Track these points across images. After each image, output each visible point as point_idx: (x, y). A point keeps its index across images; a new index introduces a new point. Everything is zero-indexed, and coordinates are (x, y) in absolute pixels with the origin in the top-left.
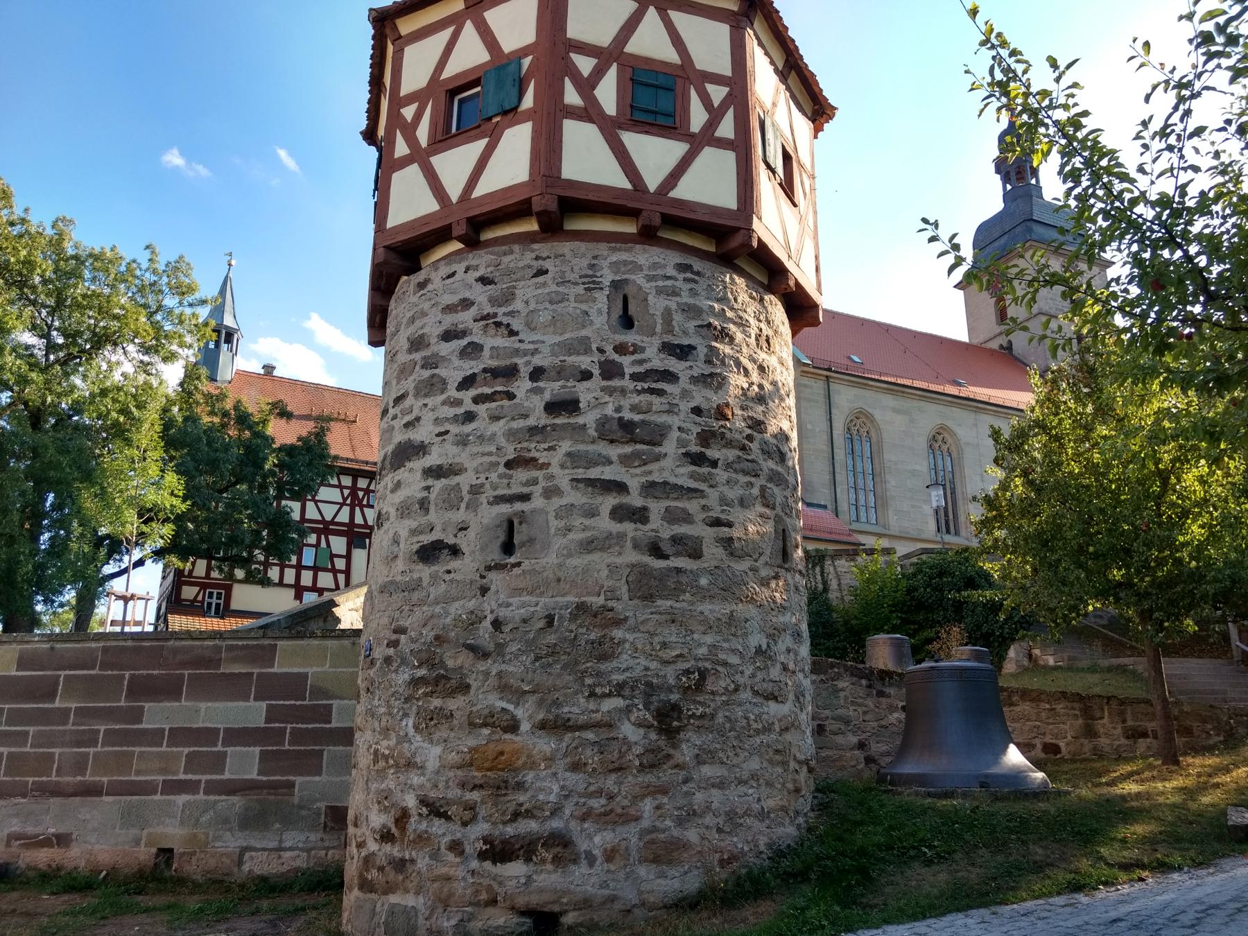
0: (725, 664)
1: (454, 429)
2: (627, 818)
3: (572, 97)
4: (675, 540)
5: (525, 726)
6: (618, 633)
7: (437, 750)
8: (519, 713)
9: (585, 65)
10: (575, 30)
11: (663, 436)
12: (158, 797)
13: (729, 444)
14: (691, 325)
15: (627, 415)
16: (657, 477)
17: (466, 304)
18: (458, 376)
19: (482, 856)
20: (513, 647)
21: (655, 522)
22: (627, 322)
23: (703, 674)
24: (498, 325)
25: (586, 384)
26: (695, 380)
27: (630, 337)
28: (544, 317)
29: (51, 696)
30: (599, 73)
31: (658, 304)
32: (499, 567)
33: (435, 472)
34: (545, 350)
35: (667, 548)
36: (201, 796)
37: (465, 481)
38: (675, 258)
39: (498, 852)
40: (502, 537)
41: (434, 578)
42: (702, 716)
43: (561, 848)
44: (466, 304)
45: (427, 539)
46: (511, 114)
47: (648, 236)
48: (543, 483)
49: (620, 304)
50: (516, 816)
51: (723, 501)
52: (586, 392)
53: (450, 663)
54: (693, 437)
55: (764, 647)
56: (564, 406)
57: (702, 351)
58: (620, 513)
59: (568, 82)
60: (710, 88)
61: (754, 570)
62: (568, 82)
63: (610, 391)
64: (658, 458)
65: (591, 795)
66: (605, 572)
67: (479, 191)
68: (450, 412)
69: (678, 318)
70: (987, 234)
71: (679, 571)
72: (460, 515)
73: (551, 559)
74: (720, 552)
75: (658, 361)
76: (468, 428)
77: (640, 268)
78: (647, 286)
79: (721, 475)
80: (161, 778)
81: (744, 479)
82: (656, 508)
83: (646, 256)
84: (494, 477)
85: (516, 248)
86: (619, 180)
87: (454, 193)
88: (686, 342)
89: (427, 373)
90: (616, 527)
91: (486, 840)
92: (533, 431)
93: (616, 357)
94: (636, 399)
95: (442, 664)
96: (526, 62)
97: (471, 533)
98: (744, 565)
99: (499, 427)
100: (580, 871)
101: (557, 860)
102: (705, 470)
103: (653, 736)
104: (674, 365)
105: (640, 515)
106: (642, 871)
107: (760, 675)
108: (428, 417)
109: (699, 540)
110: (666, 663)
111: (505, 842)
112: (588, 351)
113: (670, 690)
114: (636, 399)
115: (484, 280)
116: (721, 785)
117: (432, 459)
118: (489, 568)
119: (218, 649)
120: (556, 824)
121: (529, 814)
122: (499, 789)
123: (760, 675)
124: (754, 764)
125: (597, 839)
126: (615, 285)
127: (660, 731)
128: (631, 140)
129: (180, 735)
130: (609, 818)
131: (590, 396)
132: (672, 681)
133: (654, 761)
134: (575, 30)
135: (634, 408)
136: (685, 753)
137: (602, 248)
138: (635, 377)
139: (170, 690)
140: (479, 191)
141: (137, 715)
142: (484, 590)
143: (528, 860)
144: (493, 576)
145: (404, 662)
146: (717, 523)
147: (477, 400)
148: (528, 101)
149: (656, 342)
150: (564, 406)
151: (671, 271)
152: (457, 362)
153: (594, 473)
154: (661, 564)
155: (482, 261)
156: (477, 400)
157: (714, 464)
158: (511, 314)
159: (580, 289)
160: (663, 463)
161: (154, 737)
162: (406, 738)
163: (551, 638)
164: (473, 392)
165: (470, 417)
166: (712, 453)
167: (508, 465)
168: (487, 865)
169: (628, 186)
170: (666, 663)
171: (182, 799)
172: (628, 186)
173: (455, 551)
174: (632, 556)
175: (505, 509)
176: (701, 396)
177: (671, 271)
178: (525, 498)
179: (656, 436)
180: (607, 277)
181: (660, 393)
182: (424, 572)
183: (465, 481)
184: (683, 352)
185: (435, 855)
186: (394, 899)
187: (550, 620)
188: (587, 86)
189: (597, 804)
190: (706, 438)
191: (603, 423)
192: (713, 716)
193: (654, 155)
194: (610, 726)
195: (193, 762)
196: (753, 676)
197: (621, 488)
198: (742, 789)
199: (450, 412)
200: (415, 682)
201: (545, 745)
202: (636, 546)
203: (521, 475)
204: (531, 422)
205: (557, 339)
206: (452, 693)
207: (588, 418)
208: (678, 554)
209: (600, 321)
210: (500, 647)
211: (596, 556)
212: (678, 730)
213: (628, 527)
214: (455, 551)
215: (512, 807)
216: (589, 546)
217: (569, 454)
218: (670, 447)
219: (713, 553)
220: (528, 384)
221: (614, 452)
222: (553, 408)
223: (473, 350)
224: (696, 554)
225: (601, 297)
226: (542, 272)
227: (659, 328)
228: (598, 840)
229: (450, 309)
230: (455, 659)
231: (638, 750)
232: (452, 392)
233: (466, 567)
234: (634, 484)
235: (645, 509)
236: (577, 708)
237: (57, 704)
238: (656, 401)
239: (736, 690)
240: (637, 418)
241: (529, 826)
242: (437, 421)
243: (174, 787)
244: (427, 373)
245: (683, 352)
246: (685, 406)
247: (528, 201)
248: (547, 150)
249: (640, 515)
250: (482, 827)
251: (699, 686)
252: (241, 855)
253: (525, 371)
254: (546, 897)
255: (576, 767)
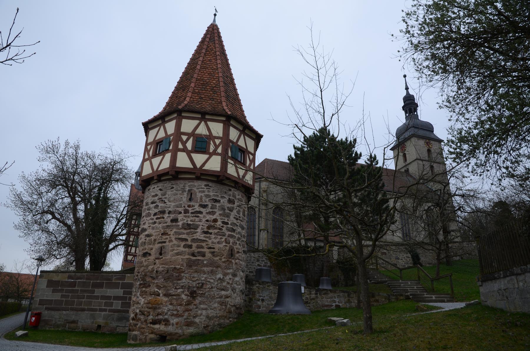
0: (209, 282)
1: (152, 226)
2: (181, 316)
3: (180, 146)
4: (198, 252)
5: (161, 295)
6: (182, 274)
7: (143, 300)
8: (160, 292)
9: (184, 138)
10: (183, 130)
11: (198, 227)
12: (98, 312)
13: (216, 228)
14: (207, 200)
15: (189, 222)
16: (195, 237)
17: (156, 195)
18: (154, 212)
19: (151, 323)
20: (160, 277)
21: (194, 248)
22: (190, 200)
23: (203, 284)
24: (162, 200)
25: (180, 215)
26: (207, 213)
27: (192, 203)
28: (172, 199)
29: (75, 286)
30: (188, 140)
31: (199, 195)
32: (158, 259)
33: (148, 236)
34: (172, 207)
35: (196, 254)
36: (107, 313)
37: (153, 238)
38: (205, 183)
39: (154, 322)
40: (159, 251)
41: (145, 260)
42: (202, 294)
43: (167, 322)
44: (156, 195)
45: (145, 251)
46: (167, 150)
47: (198, 178)
48: (169, 239)
49: (190, 195)
50: (158, 315)
51: (213, 243)
52: (180, 217)
53: (147, 280)
54: (205, 227)
55: (222, 278)
56: (175, 220)
57: (210, 206)
58: (185, 246)
59: (180, 143)
60: (216, 140)
61: (220, 259)
62: (180, 143)
63: (185, 216)
64: (196, 233)
65: (174, 310)
66: (180, 261)
67: (159, 169)
68: (151, 221)
69: (204, 198)
70: (400, 133)
71: (199, 260)
72: (151, 246)
73: (169, 257)
74: (210, 255)
75: (197, 208)
76: (154, 226)
77: (195, 186)
78: (197, 190)
79: (213, 236)
80: (98, 308)
81: (219, 237)
82: (194, 245)
83: (197, 183)
84: (159, 237)
85: (168, 182)
86: (191, 166)
87: (155, 169)
88: (206, 204)
89: (148, 211)
90: (184, 250)
91: (152, 319)
92: (168, 226)
93: (188, 208)
94: (192, 218)
95: (145, 280)
96: (172, 138)
97: (154, 250)
98: (218, 258)
99: (160, 225)
100: (170, 327)
101: (165, 325)
102: (208, 235)
103: (189, 298)
104: (202, 210)
105: (190, 247)
106: (184, 327)
107: (219, 285)
108: (147, 223)
109: (205, 252)
110: (194, 281)
111: (156, 320)
112: (181, 207)
113: (194, 287)
114: (192, 218)
115: (161, 190)
116: (206, 309)
117: (146, 233)
118: (156, 259)
119: (112, 275)
120: (166, 317)
121: (160, 314)
122: (155, 309)
123: (219, 285)
124: (216, 305)
125: (175, 320)
126: (189, 190)
127: (191, 297)
128: (193, 155)
129: (103, 297)
130: (177, 316)
131: (181, 218)
132: (194, 285)
133: (189, 303)
134: (183, 130)
135: (191, 221)
136: (197, 301)
137: (187, 182)
138: (192, 213)
139: (100, 286)
140: (159, 169)
141: (93, 292)
142: (155, 264)
143: (160, 324)
144: (157, 261)
145: (139, 280)
146: (210, 248)
147: (157, 219)
148: (171, 148)
149: (198, 204)
150: (175, 220)
151: (203, 187)
152: (153, 209)
153: (180, 236)
154: (195, 258)
155: (160, 185)
156: (157, 219)
157: (211, 234)
158: (165, 198)
159: (181, 192)
160: (197, 234)
161: (97, 297)
162: (138, 297)
163: (168, 275)
164: (156, 217)
165: (155, 223)
166: (210, 231)
167: (162, 234)
168: (152, 325)
169: (192, 167)
170: (194, 281)
171: (103, 313)
172: (192, 167)
173: (150, 254)
174: (187, 257)
175: (160, 245)
176: (209, 217)
177: (203, 187)
178: (165, 242)
179: (196, 227)
180: (187, 189)
181: (198, 217)
182: (144, 259)
183: (153, 238)
184: (205, 206)
185: (142, 323)
186: (134, 333)
187: (168, 271)
188: (184, 143)
189: (175, 312)
190: (209, 227)
191: (183, 224)
192: (204, 294)
193: (199, 159)
194: (179, 295)
195: (106, 304)
196: (217, 285)
197: (186, 240)
198: (211, 311)
199: (151, 221)
200: (140, 284)
201: (165, 299)
202: (188, 254)
203: (164, 237)
204: (168, 224)
205: (175, 204)
206: (146, 287)
207: (180, 223)
208: (199, 256)
209: (184, 199)
210: (157, 277)
211: (179, 256)
212: (195, 297)
213: (187, 249)
214: (150, 254)
215: (157, 313)
216: (178, 254)
217: (175, 232)
218: (199, 230)
219: (208, 255)
220: (167, 215)
221: (185, 231)
222: (172, 221)
223: (157, 207)
224: (204, 256)
225: (185, 194)
226: (173, 188)
227: (199, 201)
228: (174, 320)
229: (153, 196)
230: (148, 279)
231: (185, 301)
232: (152, 217)
233: (152, 258)
234: (189, 239)
235: (191, 245)
236: (172, 292)
237: (76, 288)
238: (197, 219)
239: (212, 288)
240: (191, 223)
241: (161, 317)
242: (149, 223)
243: (101, 310)
244: (148, 211)
245: (205, 206)
246: (204, 220)
247: (168, 172)
248: (174, 160)
249: (190, 247)
250: (151, 317)
251: (202, 287)
252: (116, 328)
253: (167, 212)
254: (163, 332)
255: (171, 304)
